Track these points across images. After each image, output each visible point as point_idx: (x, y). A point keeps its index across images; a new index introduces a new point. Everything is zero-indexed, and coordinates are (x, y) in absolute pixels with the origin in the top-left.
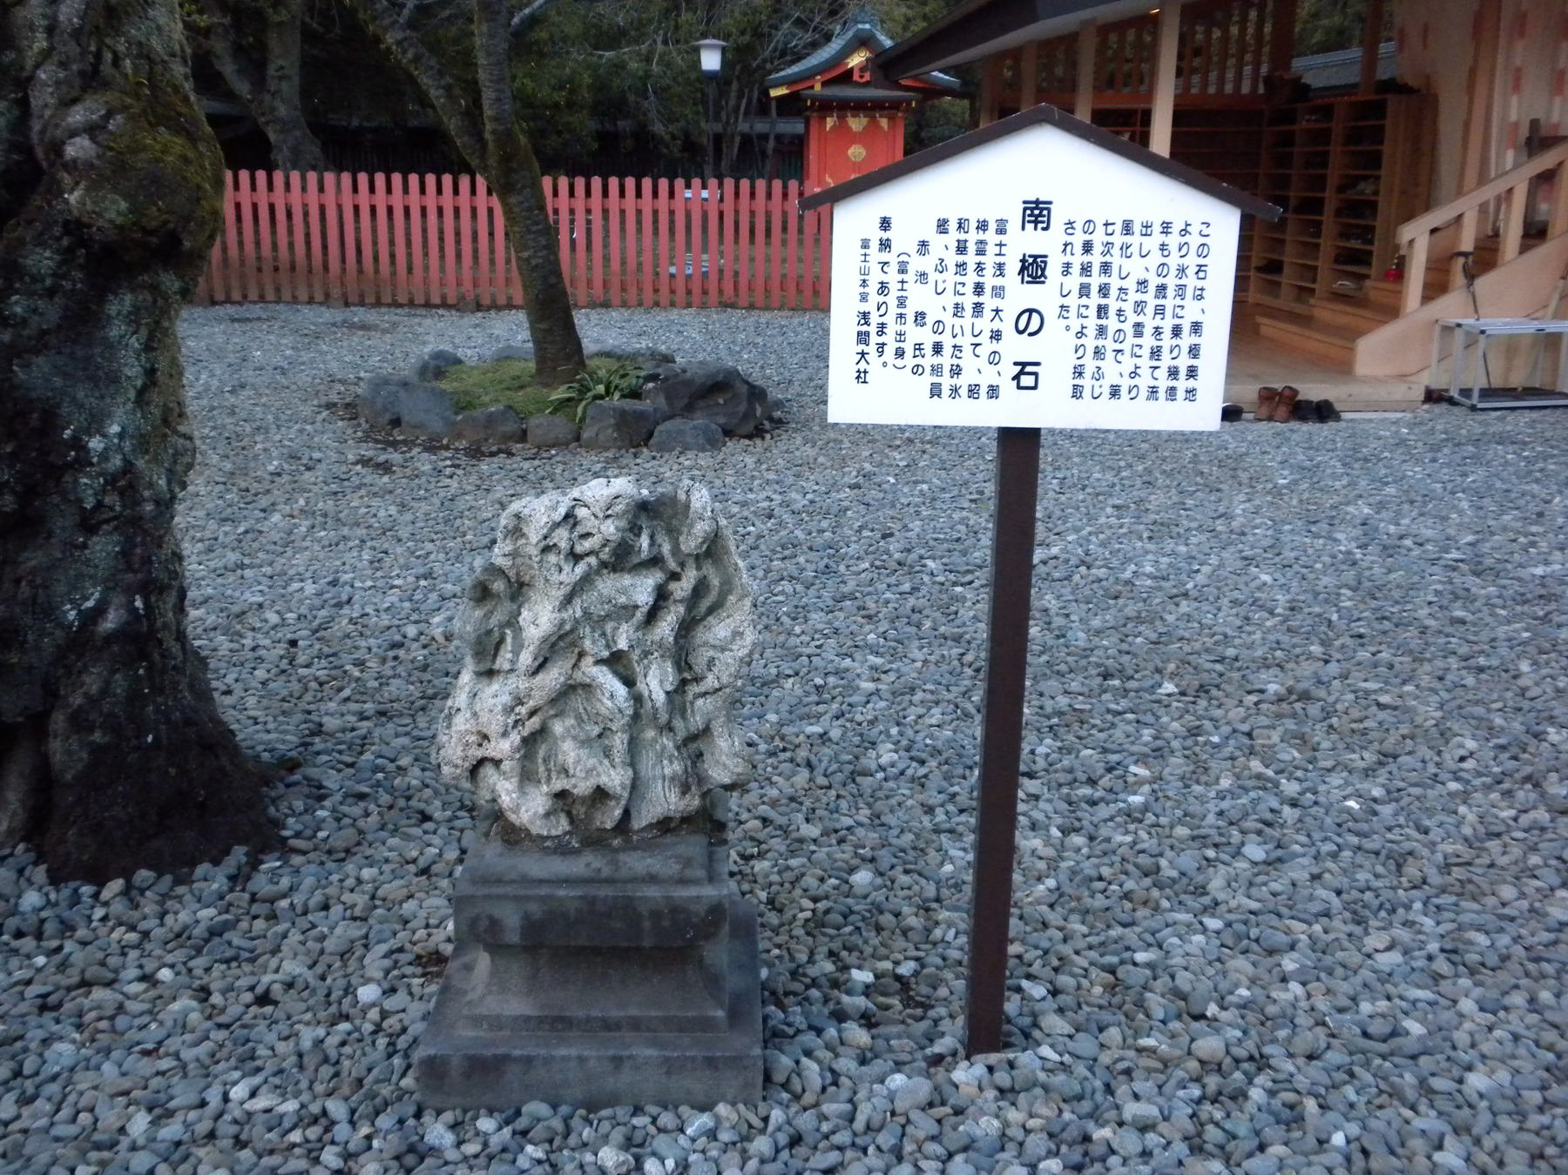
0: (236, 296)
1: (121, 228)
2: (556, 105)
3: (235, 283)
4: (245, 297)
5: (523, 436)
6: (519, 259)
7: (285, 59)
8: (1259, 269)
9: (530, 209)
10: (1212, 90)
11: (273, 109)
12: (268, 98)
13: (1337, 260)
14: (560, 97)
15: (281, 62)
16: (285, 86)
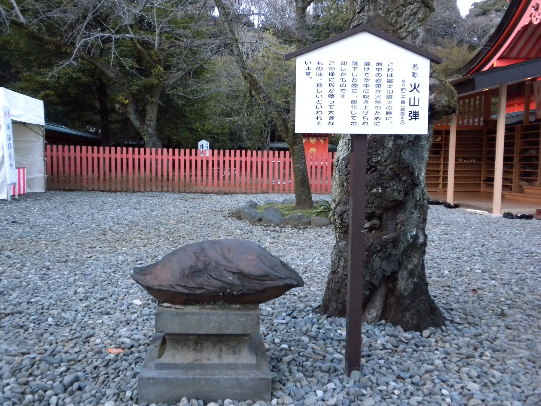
0: (142, 189)
1: (444, 106)
2: (218, 134)
3: (142, 185)
4: (145, 190)
5: (310, 223)
6: (294, 167)
7: (152, 113)
8: (484, 181)
9: (300, 151)
10: (476, 124)
11: (147, 130)
12: (145, 127)
13: (520, 175)
14: (219, 131)
15: (151, 115)
16: (152, 123)
